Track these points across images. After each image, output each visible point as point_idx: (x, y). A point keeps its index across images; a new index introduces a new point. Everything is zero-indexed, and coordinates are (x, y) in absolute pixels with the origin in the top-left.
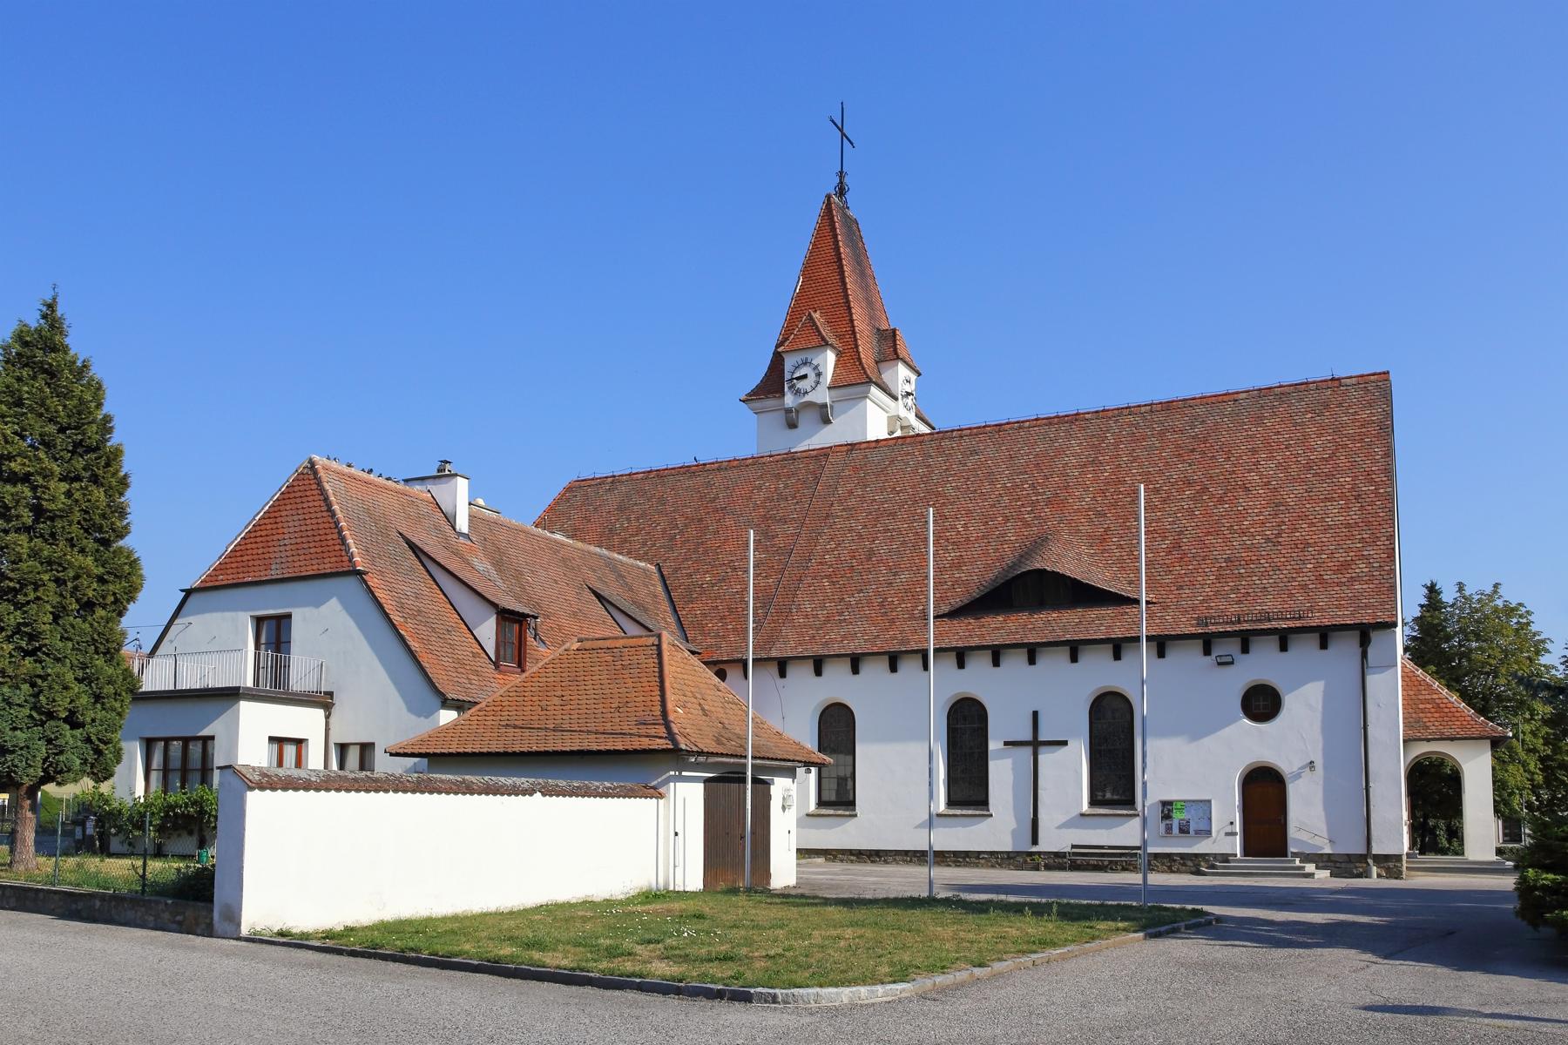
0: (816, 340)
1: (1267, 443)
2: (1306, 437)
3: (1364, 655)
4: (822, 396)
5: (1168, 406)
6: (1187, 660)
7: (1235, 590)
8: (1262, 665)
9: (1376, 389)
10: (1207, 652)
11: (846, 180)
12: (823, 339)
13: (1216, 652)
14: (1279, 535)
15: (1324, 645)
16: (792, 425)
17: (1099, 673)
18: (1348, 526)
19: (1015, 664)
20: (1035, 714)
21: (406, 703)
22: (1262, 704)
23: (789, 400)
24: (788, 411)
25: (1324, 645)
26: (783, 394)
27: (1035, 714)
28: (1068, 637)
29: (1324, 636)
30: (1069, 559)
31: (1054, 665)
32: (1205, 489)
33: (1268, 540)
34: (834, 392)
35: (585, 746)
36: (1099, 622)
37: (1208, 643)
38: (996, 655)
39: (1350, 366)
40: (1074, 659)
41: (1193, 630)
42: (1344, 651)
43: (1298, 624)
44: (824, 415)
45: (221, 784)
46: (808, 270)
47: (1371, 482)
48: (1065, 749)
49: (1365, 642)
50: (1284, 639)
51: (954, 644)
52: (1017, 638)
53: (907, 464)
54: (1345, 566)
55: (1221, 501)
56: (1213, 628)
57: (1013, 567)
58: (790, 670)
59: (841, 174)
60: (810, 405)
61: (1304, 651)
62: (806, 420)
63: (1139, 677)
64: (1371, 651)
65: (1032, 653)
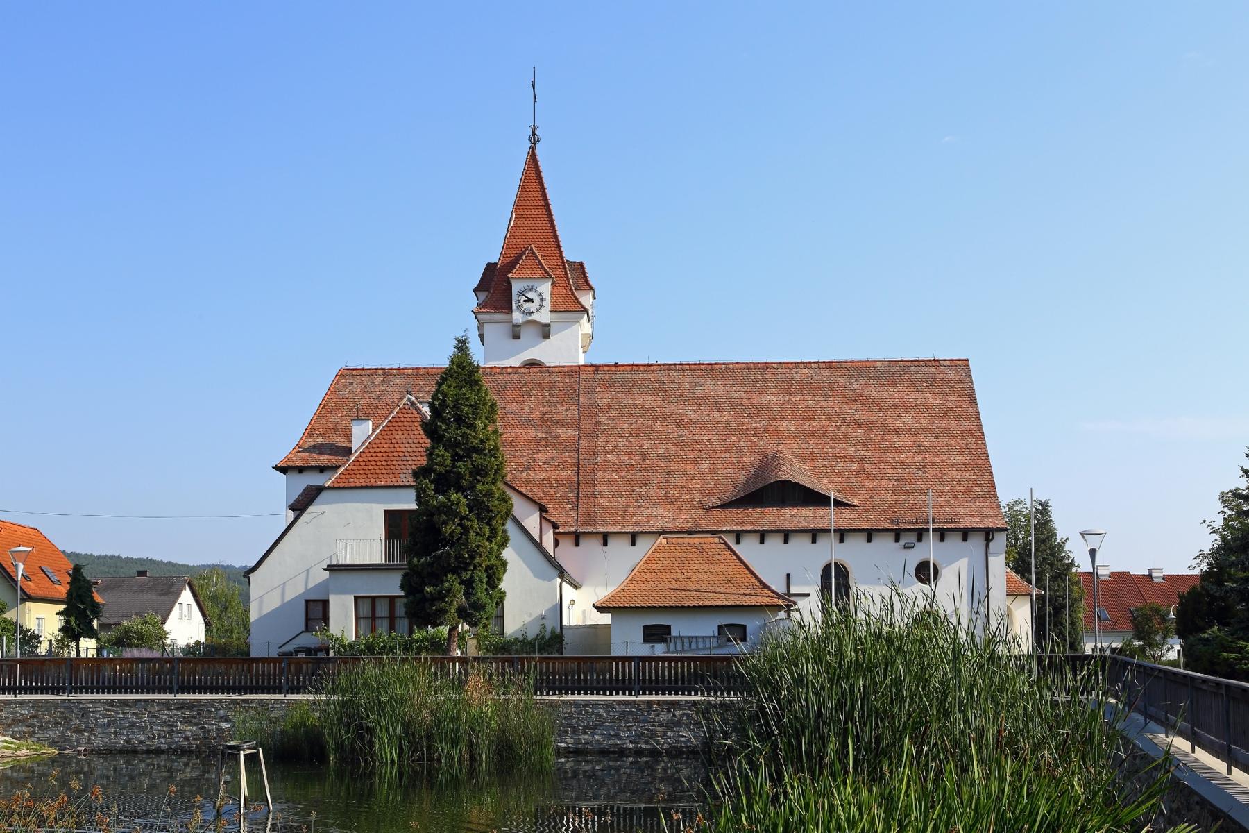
0: (539, 273)
1: (902, 400)
2: (926, 401)
3: (987, 546)
4: (544, 316)
5: (829, 365)
6: (884, 545)
7: (907, 501)
8: (930, 549)
9: (961, 369)
10: (897, 540)
11: (537, 132)
12: (546, 272)
13: (902, 542)
14: (924, 466)
15: (965, 539)
16: (516, 336)
17: (830, 551)
18: (964, 464)
19: (774, 543)
20: (788, 576)
21: (532, 571)
22: (925, 572)
23: (517, 317)
24: (516, 325)
25: (965, 539)
26: (511, 311)
27: (788, 576)
28: (812, 527)
29: (965, 534)
30: (796, 471)
31: (800, 544)
32: (870, 431)
33: (919, 469)
34: (554, 315)
35: (707, 603)
36: (831, 518)
37: (897, 534)
38: (762, 536)
39: (945, 353)
40: (814, 541)
41: (888, 526)
42: (976, 543)
43: (953, 526)
44: (545, 332)
45: (1109, 630)
46: (518, 206)
47: (972, 435)
48: (807, 599)
49: (988, 540)
50: (942, 534)
51: (735, 528)
52: (777, 526)
53: (647, 387)
54: (968, 490)
55: (883, 439)
56: (902, 526)
57: (756, 476)
58: (611, 541)
59: (534, 128)
60: (534, 322)
61: (954, 542)
62: (526, 334)
63: (852, 554)
64: (991, 544)
65: (786, 536)
